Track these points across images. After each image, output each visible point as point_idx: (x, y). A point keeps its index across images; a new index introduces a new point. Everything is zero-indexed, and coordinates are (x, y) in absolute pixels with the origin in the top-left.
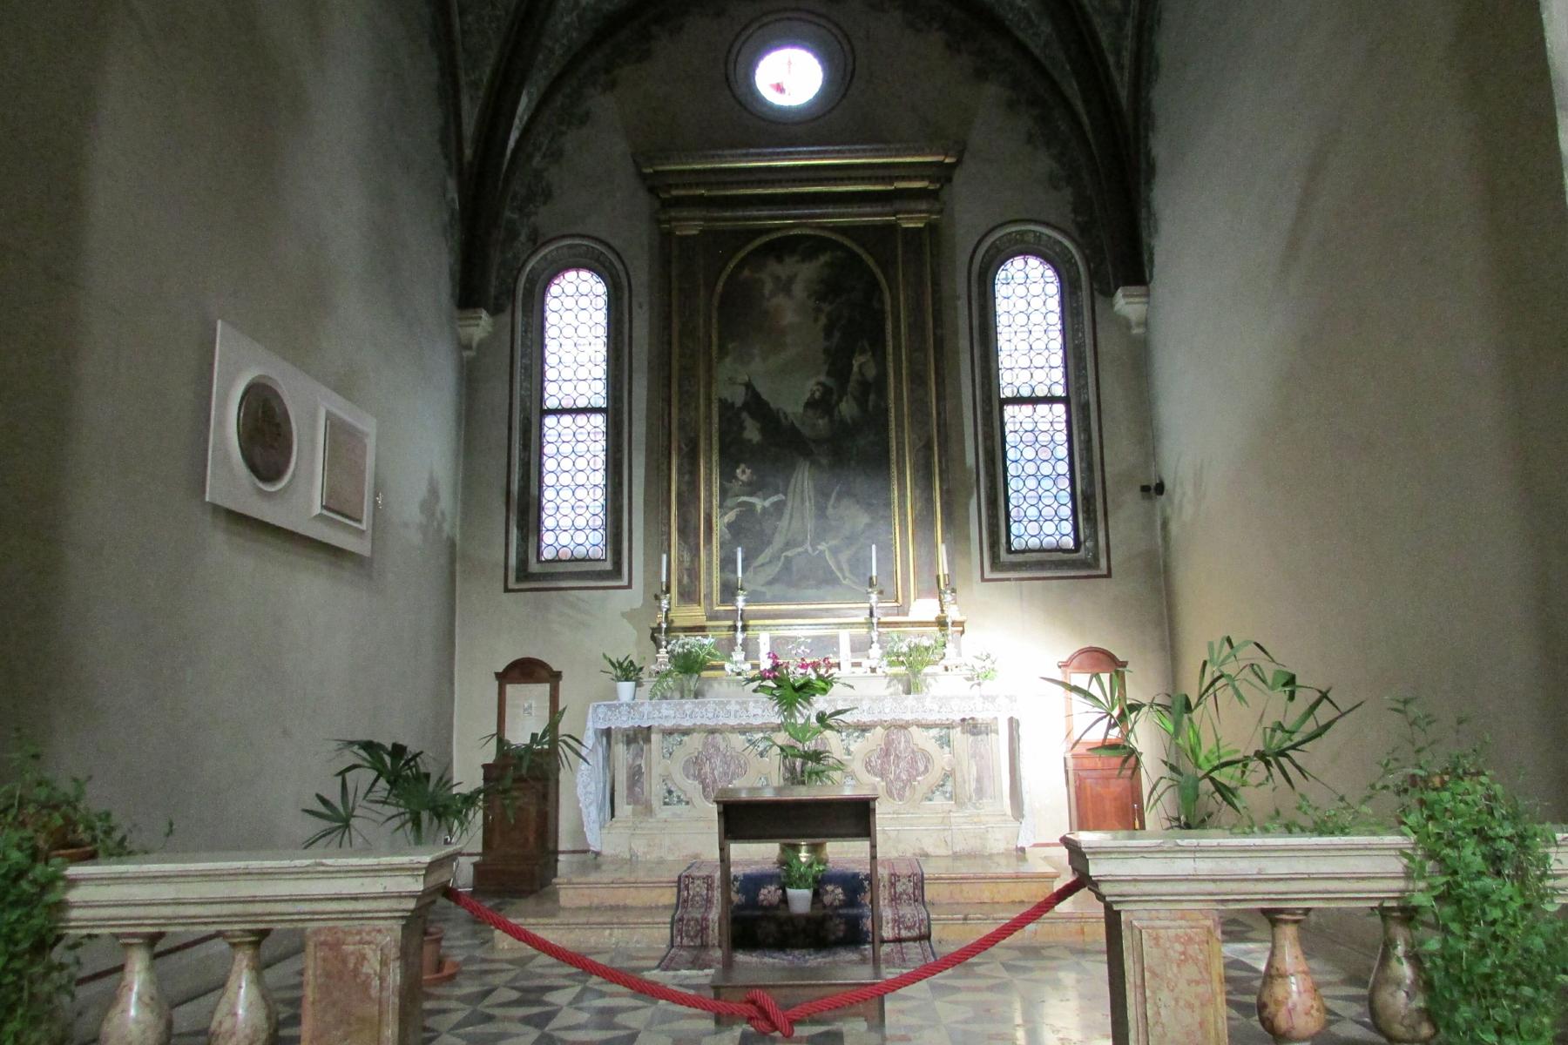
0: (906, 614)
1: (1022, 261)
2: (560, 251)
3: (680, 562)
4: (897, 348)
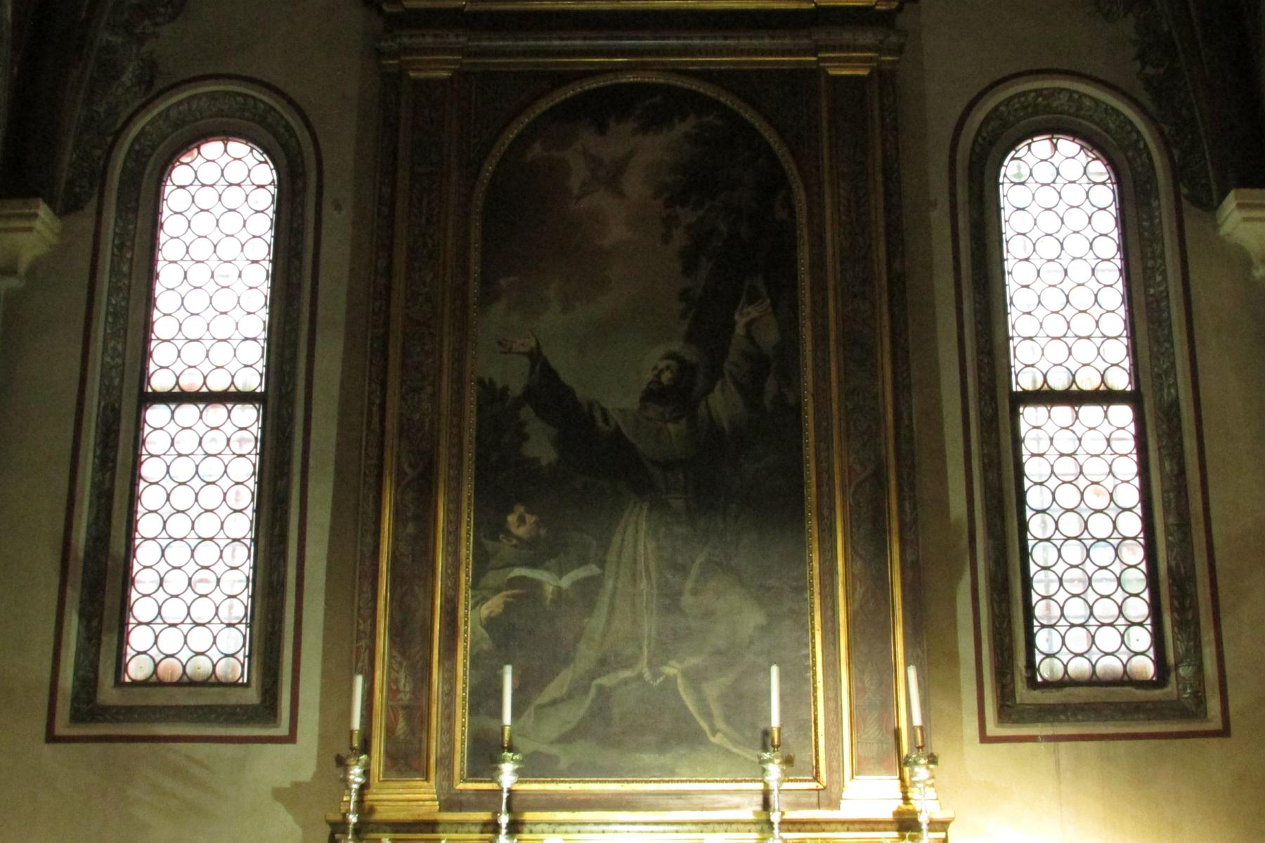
0: (834, 804)
1: (1048, 143)
2: (194, 105)
3: (393, 692)
4: (819, 287)
